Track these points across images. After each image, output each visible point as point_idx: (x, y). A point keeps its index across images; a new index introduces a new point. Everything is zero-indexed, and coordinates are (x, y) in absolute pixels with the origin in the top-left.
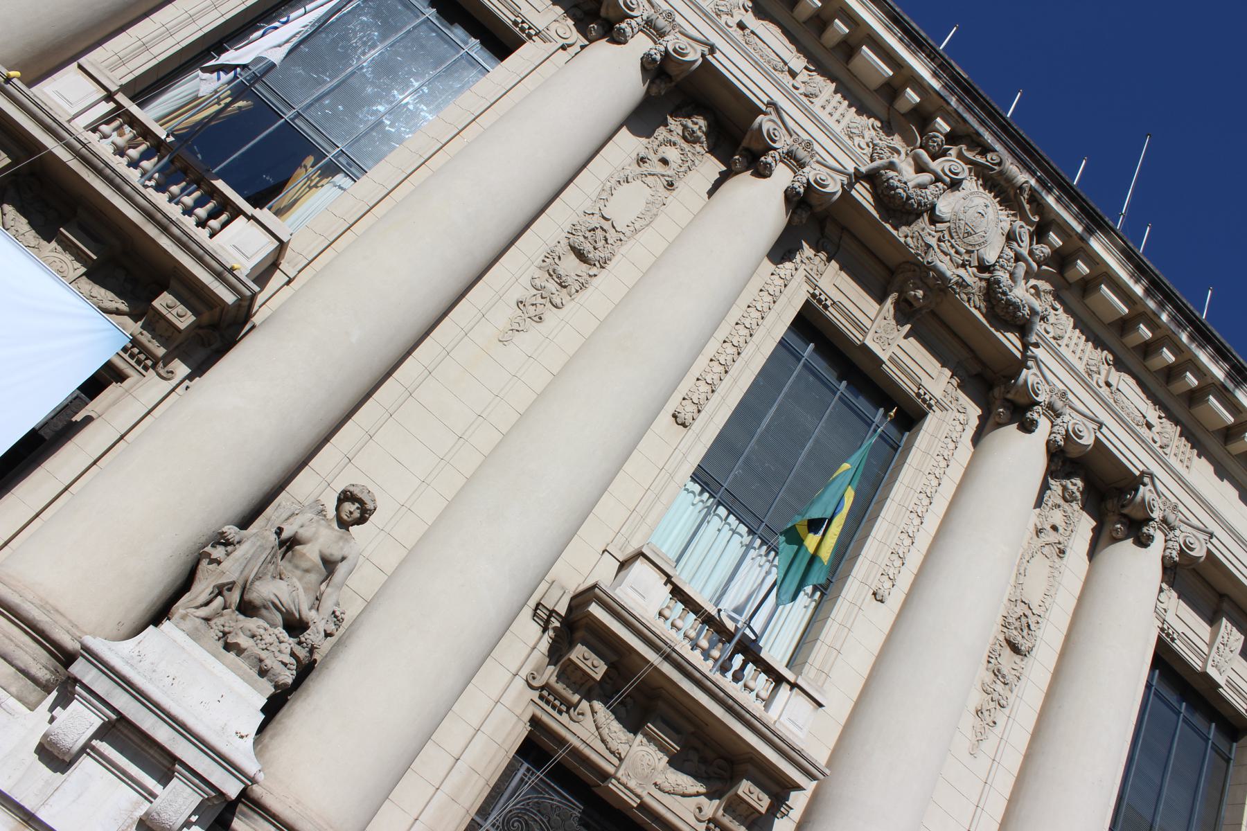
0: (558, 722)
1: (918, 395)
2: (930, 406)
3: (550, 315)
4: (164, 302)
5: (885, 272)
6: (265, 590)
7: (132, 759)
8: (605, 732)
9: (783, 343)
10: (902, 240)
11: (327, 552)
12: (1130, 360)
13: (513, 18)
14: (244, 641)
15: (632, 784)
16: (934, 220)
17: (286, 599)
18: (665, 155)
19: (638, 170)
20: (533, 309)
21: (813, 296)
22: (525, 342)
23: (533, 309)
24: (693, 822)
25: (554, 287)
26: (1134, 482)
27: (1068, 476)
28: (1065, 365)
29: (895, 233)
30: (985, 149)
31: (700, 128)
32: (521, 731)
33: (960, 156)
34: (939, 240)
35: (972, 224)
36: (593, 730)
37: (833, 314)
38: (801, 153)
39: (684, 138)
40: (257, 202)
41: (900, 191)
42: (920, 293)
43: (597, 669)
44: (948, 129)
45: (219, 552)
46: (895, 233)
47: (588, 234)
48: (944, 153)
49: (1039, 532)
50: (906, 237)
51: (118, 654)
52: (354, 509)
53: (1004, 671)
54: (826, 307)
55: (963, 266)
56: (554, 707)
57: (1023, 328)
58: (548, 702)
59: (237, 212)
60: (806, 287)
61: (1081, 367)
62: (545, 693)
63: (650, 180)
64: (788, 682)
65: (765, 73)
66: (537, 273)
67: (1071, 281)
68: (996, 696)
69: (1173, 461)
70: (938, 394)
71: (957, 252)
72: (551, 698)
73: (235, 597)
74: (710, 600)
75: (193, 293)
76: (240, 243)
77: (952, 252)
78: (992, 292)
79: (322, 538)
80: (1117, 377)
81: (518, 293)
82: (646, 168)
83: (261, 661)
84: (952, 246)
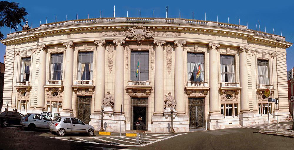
0: (132, 96)
3: (112, 69)
4: (90, 90)
5: (137, 42)
6: (107, 102)
9: (131, 55)
16: (135, 36)
17: (108, 101)
20: (110, 70)
23: (110, 70)
25: (110, 67)
28: (159, 37)
30: (135, 26)
35: (139, 34)
36: (134, 95)
40: (89, 80)
49: (167, 52)
51: (164, 112)
52: (109, 93)
57: (151, 37)
59: (88, 81)
61: (161, 36)
65: (115, 37)
69: (178, 36)
70: (148, 48)
75: (91, 88)
76: (90, 84)
78: (146, 37)
79: (108, 96)
80: (166, 33)
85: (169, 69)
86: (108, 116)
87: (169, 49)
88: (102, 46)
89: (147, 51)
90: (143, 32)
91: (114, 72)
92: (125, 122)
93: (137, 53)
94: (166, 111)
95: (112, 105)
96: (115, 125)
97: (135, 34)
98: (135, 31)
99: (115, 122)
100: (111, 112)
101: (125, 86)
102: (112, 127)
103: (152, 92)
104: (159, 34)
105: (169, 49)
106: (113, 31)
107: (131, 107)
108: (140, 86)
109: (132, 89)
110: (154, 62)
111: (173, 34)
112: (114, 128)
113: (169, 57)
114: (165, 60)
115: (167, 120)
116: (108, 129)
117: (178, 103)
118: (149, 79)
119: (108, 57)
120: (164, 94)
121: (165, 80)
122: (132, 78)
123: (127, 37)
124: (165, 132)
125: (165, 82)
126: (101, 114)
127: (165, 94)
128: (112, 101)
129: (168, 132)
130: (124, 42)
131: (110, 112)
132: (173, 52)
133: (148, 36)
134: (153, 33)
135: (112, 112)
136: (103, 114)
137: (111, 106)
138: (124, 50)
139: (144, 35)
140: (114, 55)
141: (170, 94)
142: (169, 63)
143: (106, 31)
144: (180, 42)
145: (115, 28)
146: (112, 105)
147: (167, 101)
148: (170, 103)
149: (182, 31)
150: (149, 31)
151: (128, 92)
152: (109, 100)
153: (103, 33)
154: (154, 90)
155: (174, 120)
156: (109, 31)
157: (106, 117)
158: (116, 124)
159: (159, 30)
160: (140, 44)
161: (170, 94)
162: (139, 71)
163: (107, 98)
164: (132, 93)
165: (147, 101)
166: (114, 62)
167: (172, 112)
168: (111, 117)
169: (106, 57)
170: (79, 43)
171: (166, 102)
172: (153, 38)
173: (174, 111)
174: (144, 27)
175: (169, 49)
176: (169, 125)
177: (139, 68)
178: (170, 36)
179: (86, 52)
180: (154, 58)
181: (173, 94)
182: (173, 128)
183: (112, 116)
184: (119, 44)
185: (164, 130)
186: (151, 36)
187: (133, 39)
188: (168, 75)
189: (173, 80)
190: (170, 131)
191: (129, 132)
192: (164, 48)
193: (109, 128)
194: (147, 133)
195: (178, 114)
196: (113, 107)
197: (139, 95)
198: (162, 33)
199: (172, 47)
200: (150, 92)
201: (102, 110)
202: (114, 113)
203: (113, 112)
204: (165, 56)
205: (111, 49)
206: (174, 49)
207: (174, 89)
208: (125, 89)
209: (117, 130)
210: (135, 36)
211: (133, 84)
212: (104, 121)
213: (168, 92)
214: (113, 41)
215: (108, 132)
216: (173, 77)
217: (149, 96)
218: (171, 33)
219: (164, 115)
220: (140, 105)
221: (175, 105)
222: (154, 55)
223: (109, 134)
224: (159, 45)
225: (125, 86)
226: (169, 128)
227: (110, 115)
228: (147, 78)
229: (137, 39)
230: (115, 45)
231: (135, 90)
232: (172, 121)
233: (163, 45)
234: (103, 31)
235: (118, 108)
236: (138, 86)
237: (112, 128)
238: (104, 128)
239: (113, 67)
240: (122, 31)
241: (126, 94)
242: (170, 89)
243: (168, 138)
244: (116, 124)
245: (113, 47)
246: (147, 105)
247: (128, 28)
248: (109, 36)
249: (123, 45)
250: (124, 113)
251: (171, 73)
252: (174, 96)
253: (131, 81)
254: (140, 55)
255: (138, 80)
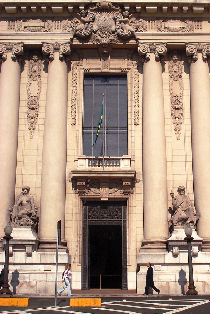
1: (122, 71)
2: (127, 71)
6: (20, 214)
7: (121, 231)
8: (94, 191)
9: (85, 85)
10: (92, 43)
11: (26, 200)
12: (169, 15)
13: (121, 70)
14: (22, 223)
15: (104, 197)
16: (95, 32)
18: (34, 70)
19: (31, 79)
20: (32, 128)
21: (84, 71)
22: (35, 135)
23: (32, 128)
24: (121, 195)
25: (32, 119)
26: (184, 47)
27: (172, 57)
28: (152, 36)
29: (89, 43)
31: (36, 57)
32: (80, 203)
33: (91, 11)
34: (100, 35)
36: (92, 193)
37: (92, 71)
38: (57, 47)
39: (35, 62)
41: (82, 35)
42: (105, 51)
43: (84, 184)
44: (84, 7)
45: (11, 213)
46: (89, 43)
47: (31, 103)
48: (88, 13)
50: (92, 42)
51: (169, 239)
52: (26, 191)
53: (177, 116)
54: (89, 71)
55: (109, 36)
56: (83, 194)
57: (133, 37)
58: (81, 194)
60: (81, 70)
61: (155, 31)
62: (79, 193)
63: (35, 79)
64: (121, 159)
66: (28, 120)
67: (140, 11)
68: (177, 123)
69: (196, 31)
71: (106, 34)
72: (81, 193)
73: (17, 218)
74: (74, 173)
77: (105, 35)
79: (24, 199)
81: (27, 127)
82: (32, 76)
83: (26, 224)
84: (104, 34)
85: (177, 121)
86: (23, 254)
87: (175, 67)
88: (14, 59)
89: (123, 76)
90: (113, 22)
91: (41, 134)
92: (68, 266)
93: (99, 82)
94: (174, 237)
95: (35, 223)
96: (43, 277)
97: (95, 27)
98: (94, 19)
99: (42, 268)
100: (31, 243)
101: (69, 170)
102: (34, 283)
103: (137, 184)
104: (151, 27)
105: (175, 67)
106: (44, 19)
107: (84, 227)
108: (107, 169)
109: (86, 179)
110: (141, 104)
111: (182, 24)
112: (40, 285)
113: (177, 92)
114: (167, 98)
115: (176, 260)
116: (22, 290)
117: (202, 215)
118: (129, 151)
119: (28, 90)
120: (167, 191)
121: (169, 152)
122: (86, 150)
123: (76, 36)
124: (172, 293)
125: (169, 159)
126: (5, 248)
127: (169, 192)
128: (33, 211)
129: (179, 293)
130: (68, 48)
131: (28, 243)
132: (185, 76)
133: (125, 32)
134: (137, 23)
135: (34, 243)
136: (11, 248)
137: (32, 225)
138: (21, 72)
139: (116, 31)
140: (44, 86)
141: (181, 191)
142: (177, 106)
143: (25, 19)
144: (200, 48)
145: (63, 9)
146: (35, 223)
147: (175, 208)
148: (184, 215)
149: (203, 16)
150: (128, 17)
151: (75, 187)
152: (25, 210)
153: (18, 23)
154: (141, 179)
155: (194, 260)
156: (34, 18)
157: (19, 256)
158: (45, 273)
159: (150, 16)
160: (105, 57)
161: (183, 190)
162: (105, 129)
163: (21, 204)
164: (86, 190)
165: (125, 210)
166: (42, 104)
167: (189, 239)
168: (29, 255)
169: (23, 92)
170: (86, 49)
171: (172, 211)
172: (138, 37)
173: (194, 235)
174: (114, 7)
175: (175, 68)
176: (182, 273)
177: (105, 123)
178: (175, 33)
179: (106, 77)
180: (141, 92)
181: (189, 191)
182: (192, 286)
183: (35, 253)
184: (57, 56)
185: (169, 288)
186: (132, 32)
187: (91, 42)
188: (175, 139)
189: (189, 152)
190: (186, 289)
191: (79, 295)
192: (163, 65)
193: (25, 285)
194: (126, 296)
195: (206, 246)
196: (36, 229)
197: (104, 193)
198: (158, 23)
199: (181, 63)
200: (133, 186)
201: (8, 238)
202: (39, 245)
203: (36, 241)
204: (166, 87)
205: (35, 68)
206: (188, 70)
207: (190, 178)
208: (67, 179)
209: (46, 290)
210: (95, 32)
211: (89, 166)
212: (12, 268)
213: (177, 186)
214: (41, 46)
215: (23, 296)
216: (189, 146)
217: (131, 197)
218: (177, 21)
219: (168, 246)
220: (106, 221)
221: (197, 221)
222: (141, 86)
223: (25, 302)
224: (152, 56)
225: (69, 170)
226: (182, 281)
227: (29, 249)
228: (124, 149)
229: (98, 40)
230: (47, 59)
231: (95, 182)
232: (190, 264)
233: (161, 59)
234: (19, 19)
235: (49, 231)
236: (100, 169)
237: (32, 287)
238: (11, 288)
239: (40, 121)
240: (65, 18)
241: (70, 191)
242: (181, 177)
243: (181, 309)
244: (45, 273)
245: (41, 63)
246: (125, 222)
247: (79, 10)
248: (32, 33)
249: (67, 58)
250: (65, 244)
251: (182, 132)
252: (191, 197)
253: (84, 156)
254: (106, 87)
255: (102, 155)
